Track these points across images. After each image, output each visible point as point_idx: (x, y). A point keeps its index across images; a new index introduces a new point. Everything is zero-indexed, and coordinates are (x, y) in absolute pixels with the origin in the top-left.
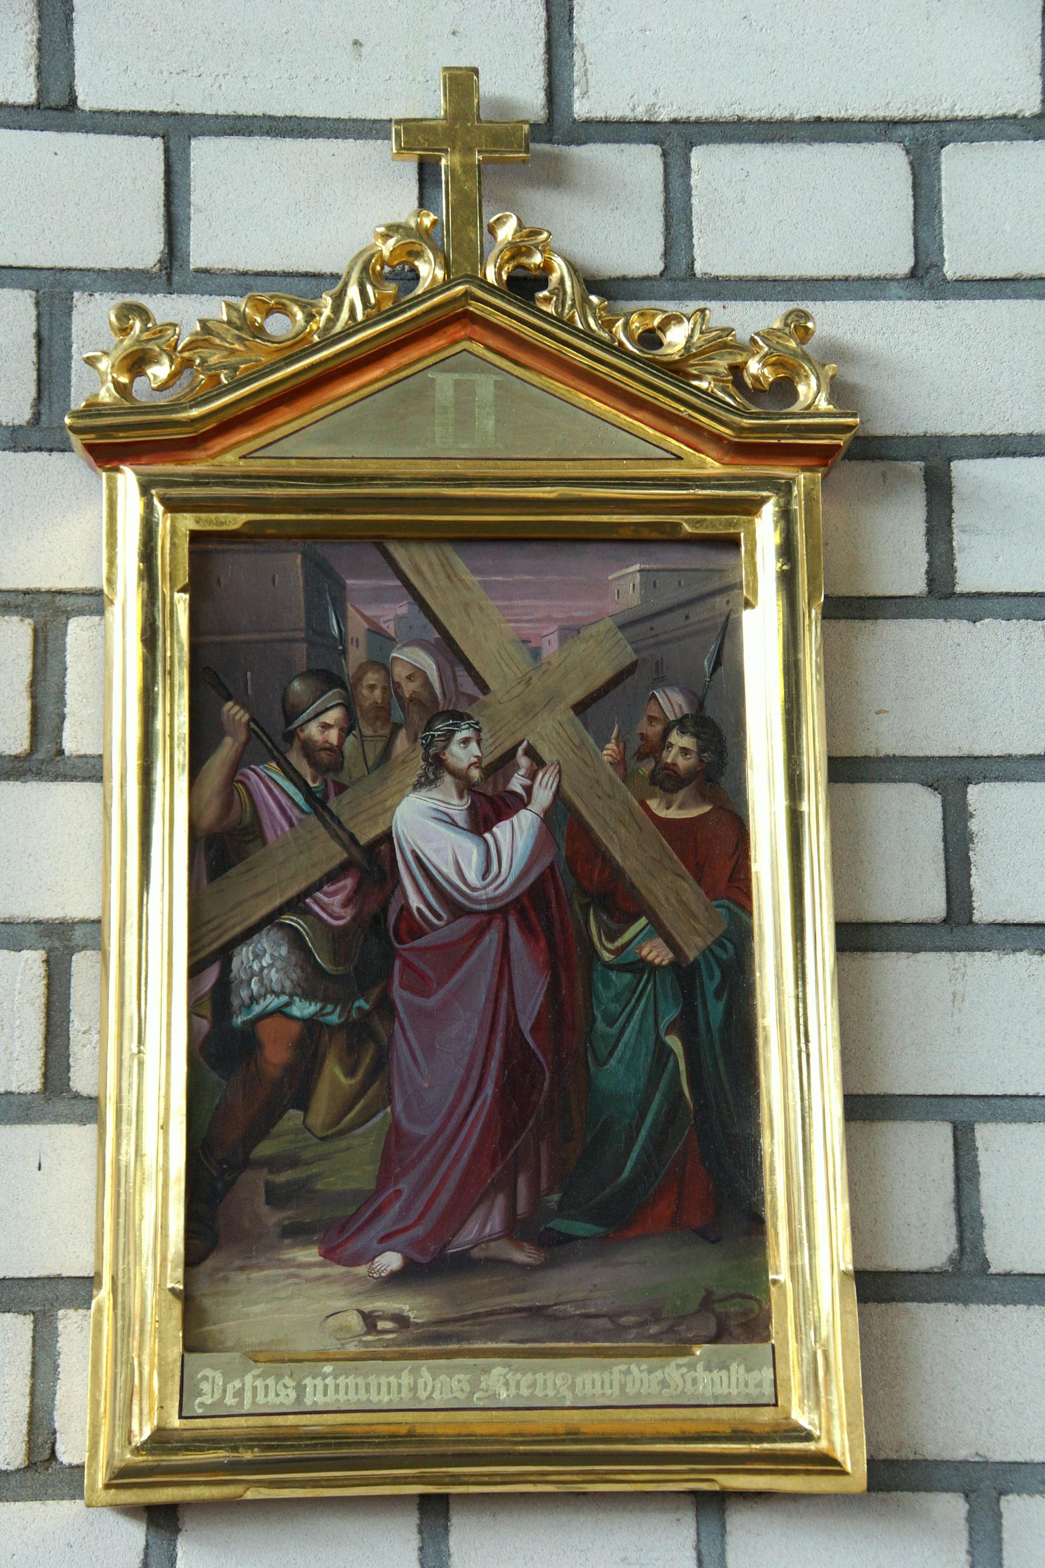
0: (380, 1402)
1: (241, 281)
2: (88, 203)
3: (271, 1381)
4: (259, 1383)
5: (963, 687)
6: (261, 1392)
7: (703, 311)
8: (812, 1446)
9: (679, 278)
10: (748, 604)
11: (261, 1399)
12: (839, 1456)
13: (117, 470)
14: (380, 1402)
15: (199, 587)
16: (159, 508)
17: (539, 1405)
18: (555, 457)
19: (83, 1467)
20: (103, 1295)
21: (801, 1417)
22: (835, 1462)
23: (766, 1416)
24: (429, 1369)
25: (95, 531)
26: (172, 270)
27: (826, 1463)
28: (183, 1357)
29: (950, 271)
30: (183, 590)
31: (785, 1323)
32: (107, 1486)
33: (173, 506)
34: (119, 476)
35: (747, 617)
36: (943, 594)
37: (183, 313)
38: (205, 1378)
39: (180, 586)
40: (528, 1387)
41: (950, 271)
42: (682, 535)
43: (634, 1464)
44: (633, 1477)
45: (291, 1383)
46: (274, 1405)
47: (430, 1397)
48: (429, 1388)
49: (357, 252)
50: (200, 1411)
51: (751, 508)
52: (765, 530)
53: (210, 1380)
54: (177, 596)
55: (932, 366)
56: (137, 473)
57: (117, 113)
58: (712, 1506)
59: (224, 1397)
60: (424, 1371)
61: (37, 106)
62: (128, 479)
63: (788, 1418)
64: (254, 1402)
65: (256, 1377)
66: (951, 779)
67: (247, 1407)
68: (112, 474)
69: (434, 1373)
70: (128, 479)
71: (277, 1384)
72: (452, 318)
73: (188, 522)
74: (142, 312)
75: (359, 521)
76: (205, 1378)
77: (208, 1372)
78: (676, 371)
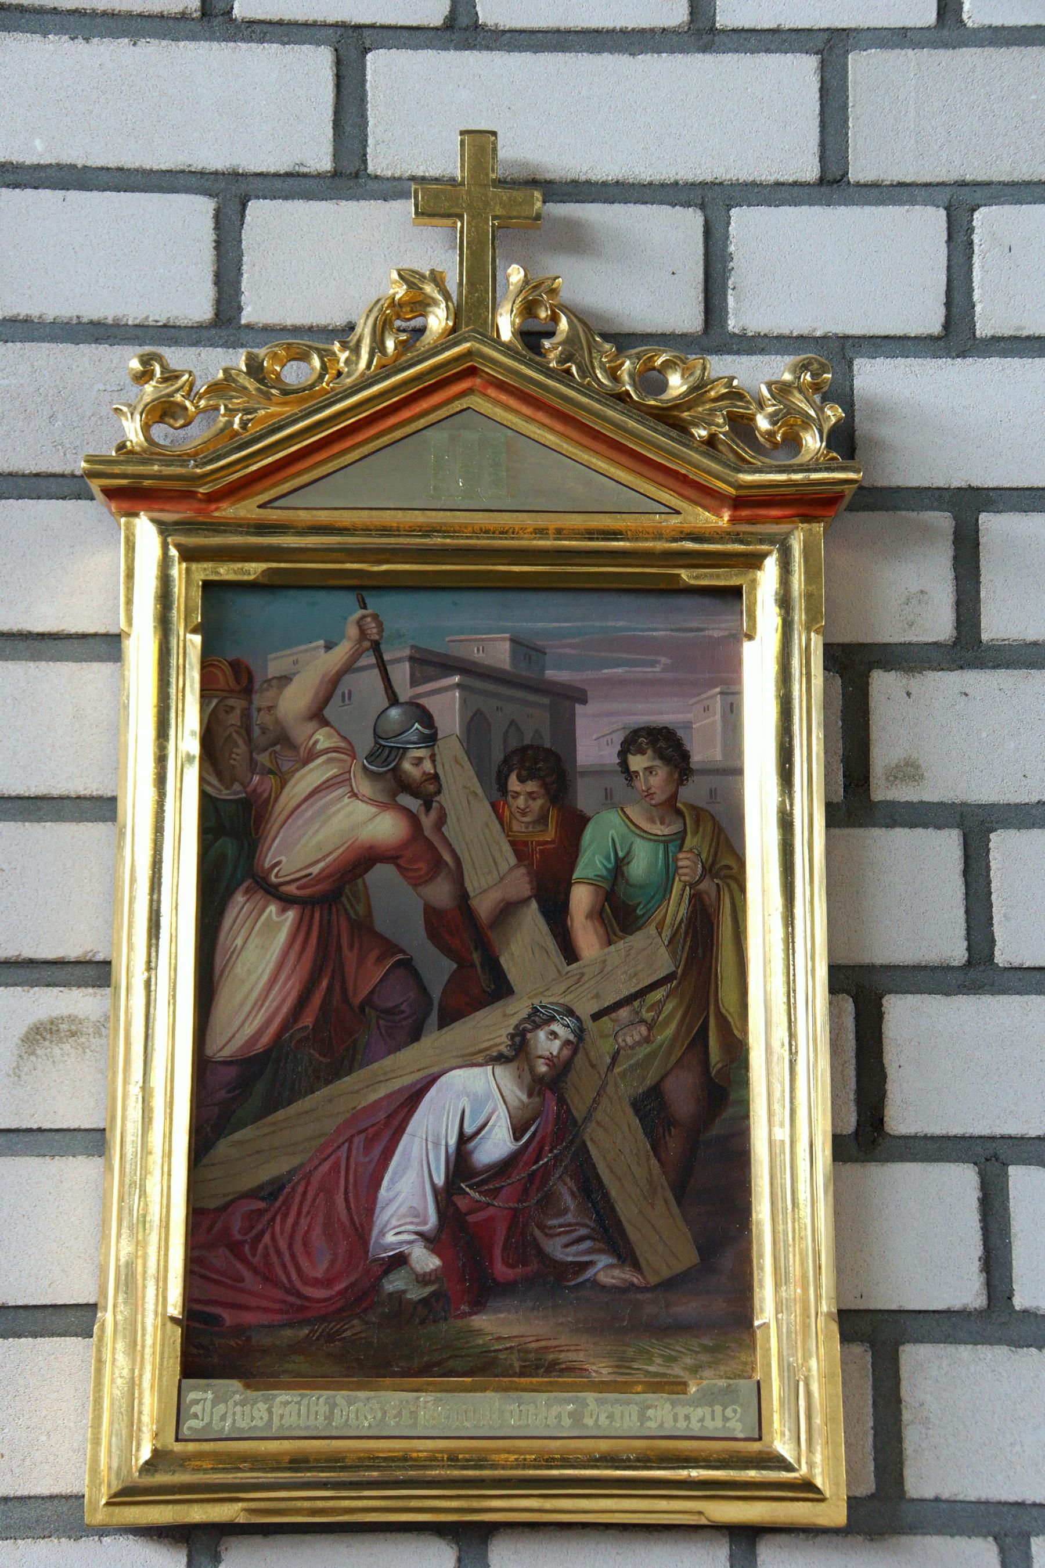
1: (269, 332)
3: (247, 1408)
4: (238, 1408)
5: (969, 735)
8: (785, 1475)
9: (714, 334)
10: (750, 637)
12: (819, 1482)
13: (136, 515)
15: (210, 630)
16: (174, 552)
17: (540, 1435)
19: (83, 1496)
20: (107, 1317)
21: (783, 1447)
22: (817, 1490)
23: (756, 1446)
25: (127, 573)
26: (225, 322)
27: (807, 1488)
28: (180, 1381)
29: (983, 329)
30: (194, 631)
32: (108, 1504)
33: (189, 555)
34: (136, 521)
35: (748, 649)
36: (968, 648)
37: (209, 363)
38: (196, 1402)
39: (191, 626)
41: (983, 329)
42: (681, 586)
43: (517, 1489)
44: (414, 1504)
45: (377, 1406)
46: (307, 1428)
47: (661, 1426)
49: (374, 301)
51: (755, 561)
52: (767, 578)
54: (189, 636)
55: (952, 418)
56: (153, 520)
58: (471, 1536)
61: (336, 174)
63: (771, 1447)
65: (236, 1404)
66: (976, 827)
67: (274, 1431)
68: (131, 519)
72: (469, 369)
73: (203, 571)
74: (159, 358)
75: (491, 571)
78: (671, 419)
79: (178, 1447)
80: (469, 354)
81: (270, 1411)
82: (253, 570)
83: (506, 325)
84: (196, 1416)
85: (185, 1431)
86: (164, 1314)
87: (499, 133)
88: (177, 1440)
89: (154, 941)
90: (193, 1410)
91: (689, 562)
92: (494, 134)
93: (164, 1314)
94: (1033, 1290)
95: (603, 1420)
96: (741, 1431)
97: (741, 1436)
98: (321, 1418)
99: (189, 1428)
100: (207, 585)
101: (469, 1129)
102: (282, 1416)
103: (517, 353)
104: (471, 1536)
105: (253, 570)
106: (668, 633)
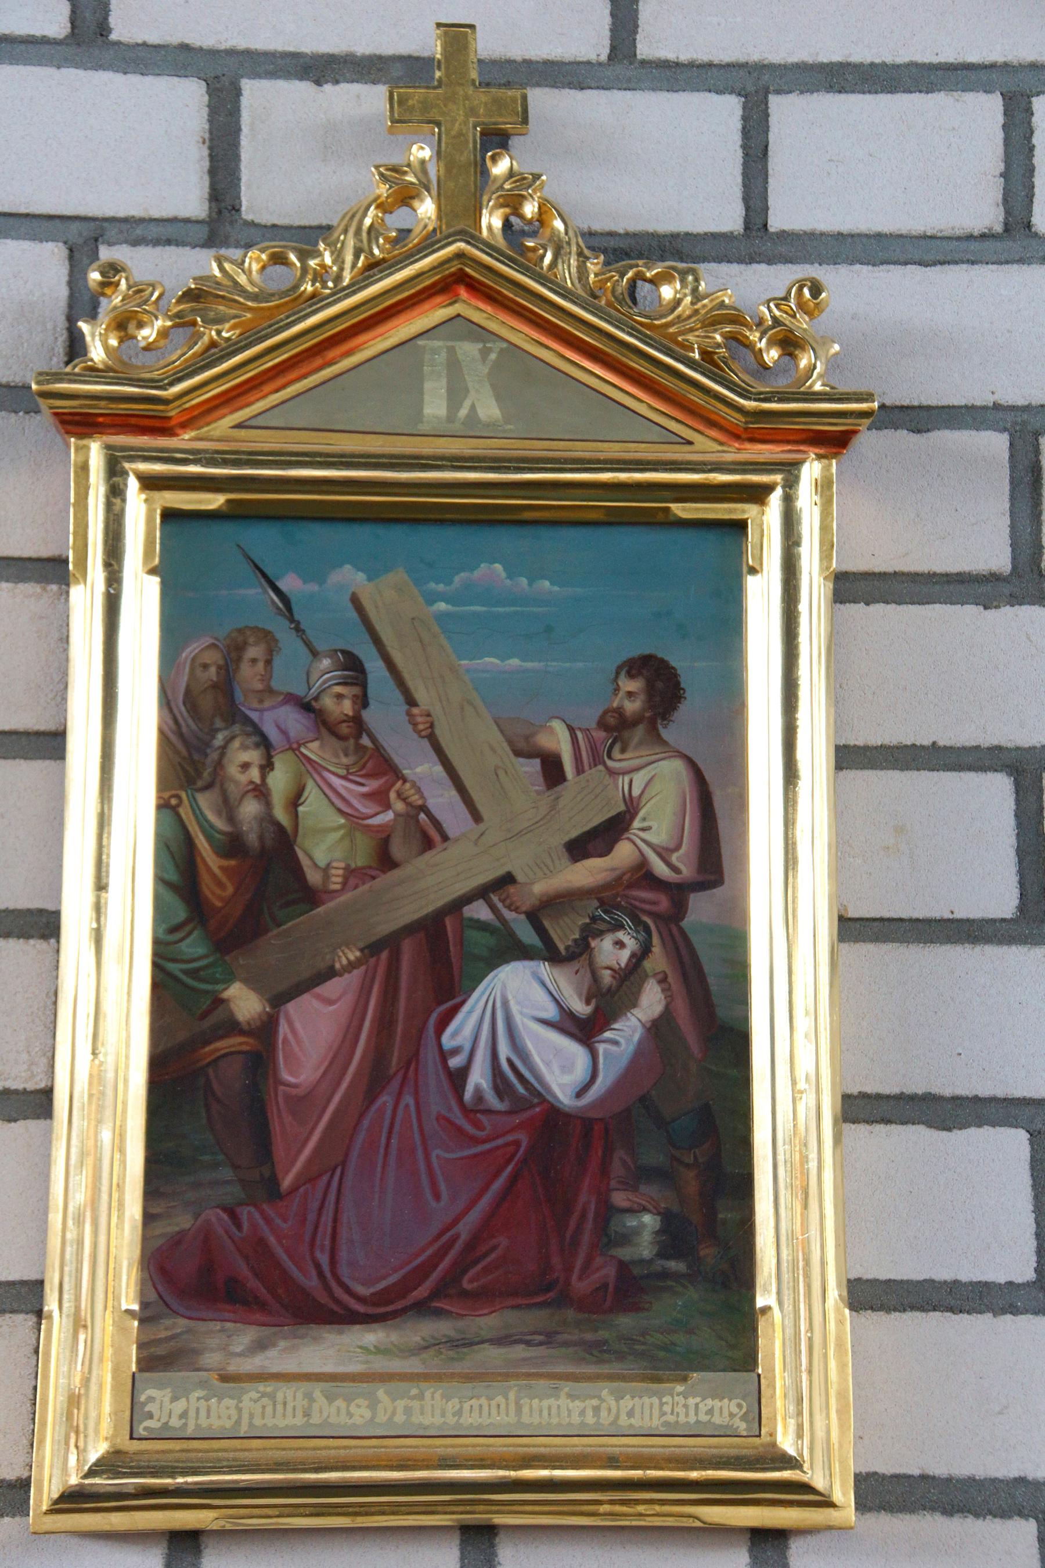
0: (210, 1426)
2: (136, 147)
6: (203, 1413)
7: (817, 290)
10: (753, 571)
11: (204, 1422)
14: (210, 1426)
16: (133, 484)
18: (345, 376)
21: (787, 1443)
24: (386, 1392)
26: (222, 220)
31: (773, 1342)
33: (150, 483)
35: (753, 584)
38: (151, 1399)
40: (706, 1414)
42: (672, 518)
48: (389, 1412)
50: (145, 1434)
51: (758, 494)
53: (158, 1402)
57: (1021, 261)
59: (617, 1417)
60: (317, 1394)
62: (96, 452)
63: (774, 1445)
64: (251, 1425)
67: (190, 1432)
69: (330, 1398)
70: (96, 452)
71: (348, 1406)
76: (151, 1399)
77: (151, 1392)
79: (136, 1446)
80: (460, 255)
81: (240, 1410)
82: (215, 501)
83: (492, 221)
84: (150, 1416)
85: (140, 1431)
86: (116, 1308)
87: (478, 28)
88: (132, 1438)
89: (106, 794)
90: (147, 1409)
91: (679, 495)
92: (472, 27)
93: (116, 1308)
94: (1044, 219)
95: (400, 1418)
96: (745, 1430)
97: (745, 1433)
98: (299, 1413)
99: (145, 1429)
100: (170, 516)
101: (551, 1012)
102: (251, 1416)
103: (502, 254)
104: (479, 1537)
105: (215, 501)
106: (226, 1237)
